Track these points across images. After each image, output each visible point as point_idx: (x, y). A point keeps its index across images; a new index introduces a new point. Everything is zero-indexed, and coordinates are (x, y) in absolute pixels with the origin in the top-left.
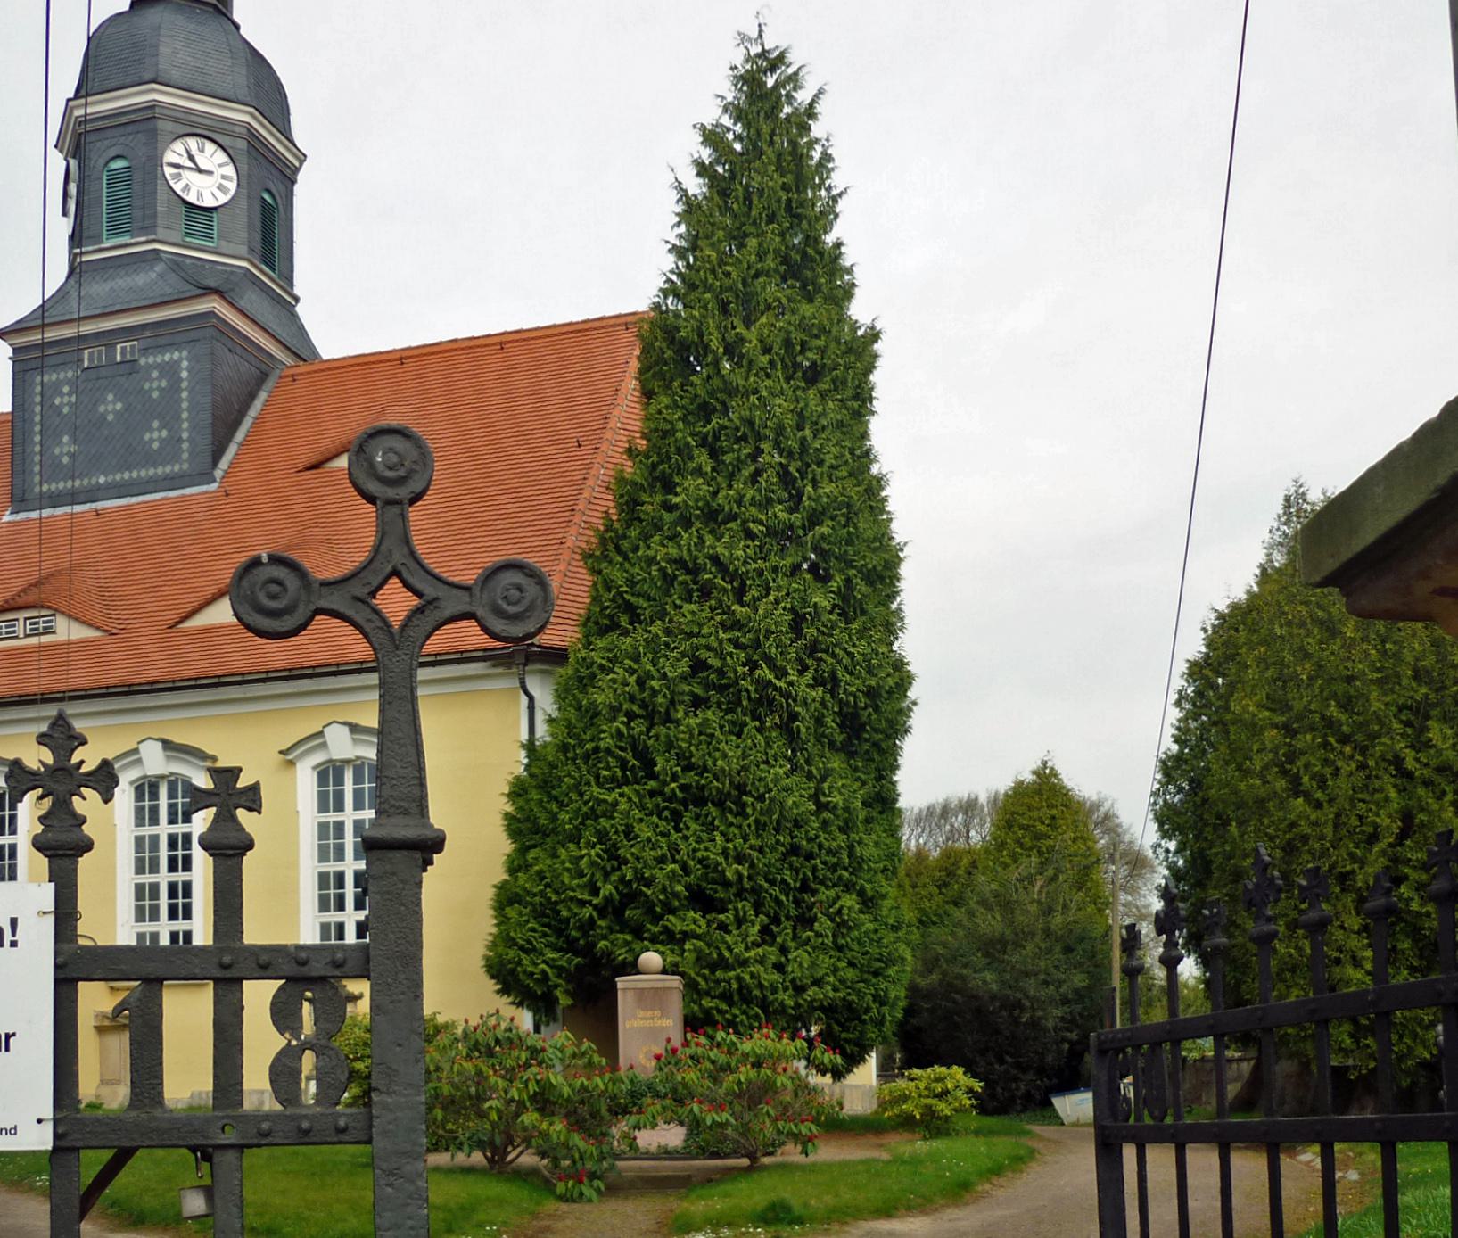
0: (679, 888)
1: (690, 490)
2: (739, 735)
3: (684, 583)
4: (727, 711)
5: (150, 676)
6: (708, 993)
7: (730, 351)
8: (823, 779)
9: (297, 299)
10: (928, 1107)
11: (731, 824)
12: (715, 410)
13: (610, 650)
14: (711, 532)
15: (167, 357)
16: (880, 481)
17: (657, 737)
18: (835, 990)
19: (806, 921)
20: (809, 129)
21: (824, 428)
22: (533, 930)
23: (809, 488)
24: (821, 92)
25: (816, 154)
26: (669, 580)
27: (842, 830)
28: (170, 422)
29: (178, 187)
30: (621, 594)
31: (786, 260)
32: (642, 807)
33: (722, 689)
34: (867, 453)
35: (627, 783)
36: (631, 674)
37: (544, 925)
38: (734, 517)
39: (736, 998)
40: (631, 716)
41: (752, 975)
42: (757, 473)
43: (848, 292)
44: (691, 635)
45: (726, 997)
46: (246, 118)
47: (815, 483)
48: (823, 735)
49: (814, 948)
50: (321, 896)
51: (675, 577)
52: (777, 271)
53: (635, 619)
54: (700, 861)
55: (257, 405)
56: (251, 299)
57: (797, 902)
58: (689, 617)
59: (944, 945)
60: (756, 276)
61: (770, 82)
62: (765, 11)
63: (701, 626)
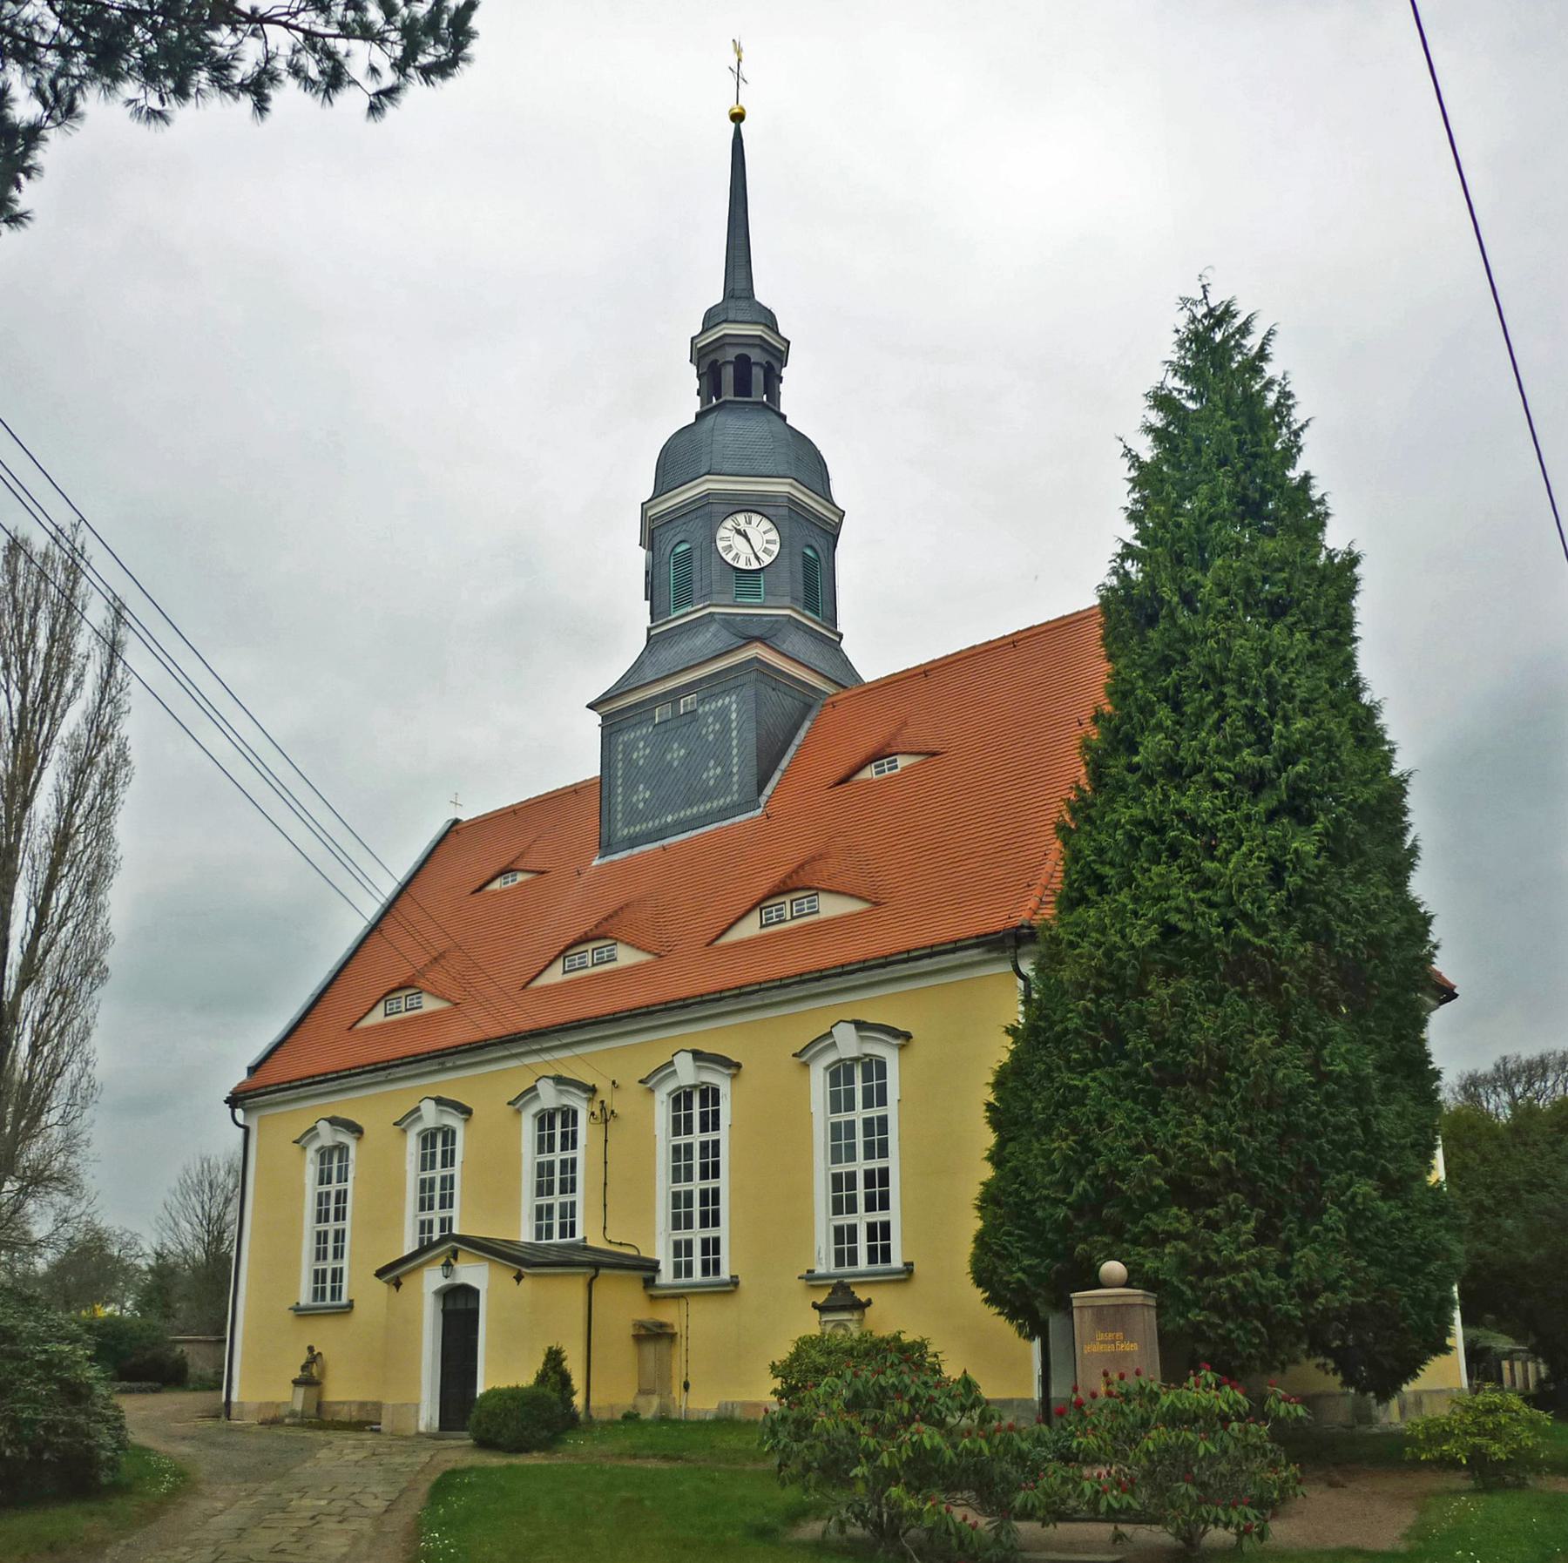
0: (1158, 1181)
1: (1152, 746)
2: (1218, 1004)
3: (1151, 845)
4: (1205, 978)
5: (683, 992)
6: (1196, 1303)
7: (1188, 600)
8: (1323, 1044)
10: (1476, 1449)
11: (1215, 1104)
12: (1174, 663)
13: (1078, 925)
14: (1176, 788)
15: (720, 703)
16: (1371, 712)
17: (1128, 1011)
18: (1355, 1294)
19: (1313, 1211)
20: (1262, 370)
21: (1292, 662)
22: (1009, 1234)
23: (1278, 727)
24: (1271, 333)
25: (1271, 398)
26: (1135, 842)
27: (1352, 1102)
28: (724, 762)
29: (729, 558)
30: (1088, 864)
31: (1243, 500)
32: (1115, 1091)
33: (1196, 955)
34: (1357, 680)
35: (1100, 1065)
36: (1099, 947)
37: (1021, 1228)
38: (1198, 769)
39: (1230, 1309)
40: (1099, 992)
41: (1246, 1282)
42: (1222, 719)
43: (1320, 523)
44: (1160, 899)
45: (1217, 1307)
46: (786, 489)
47: (1287, 721)
48: (1320, 995)
49: (1324, 1245)
50: (834, 1198)
51: (1142, 838)
52: (1234, 513)
53: (1103, 890)
54: (1181, 1148)
55: (802, 733)
56: (795, 643)
57: (1303, 1189)
58: (1157, 880)
59: (1550, 1213)
60: (1211, 520)
61: (1218, 337)
62: (1208, 273)
63: (1168, 887)
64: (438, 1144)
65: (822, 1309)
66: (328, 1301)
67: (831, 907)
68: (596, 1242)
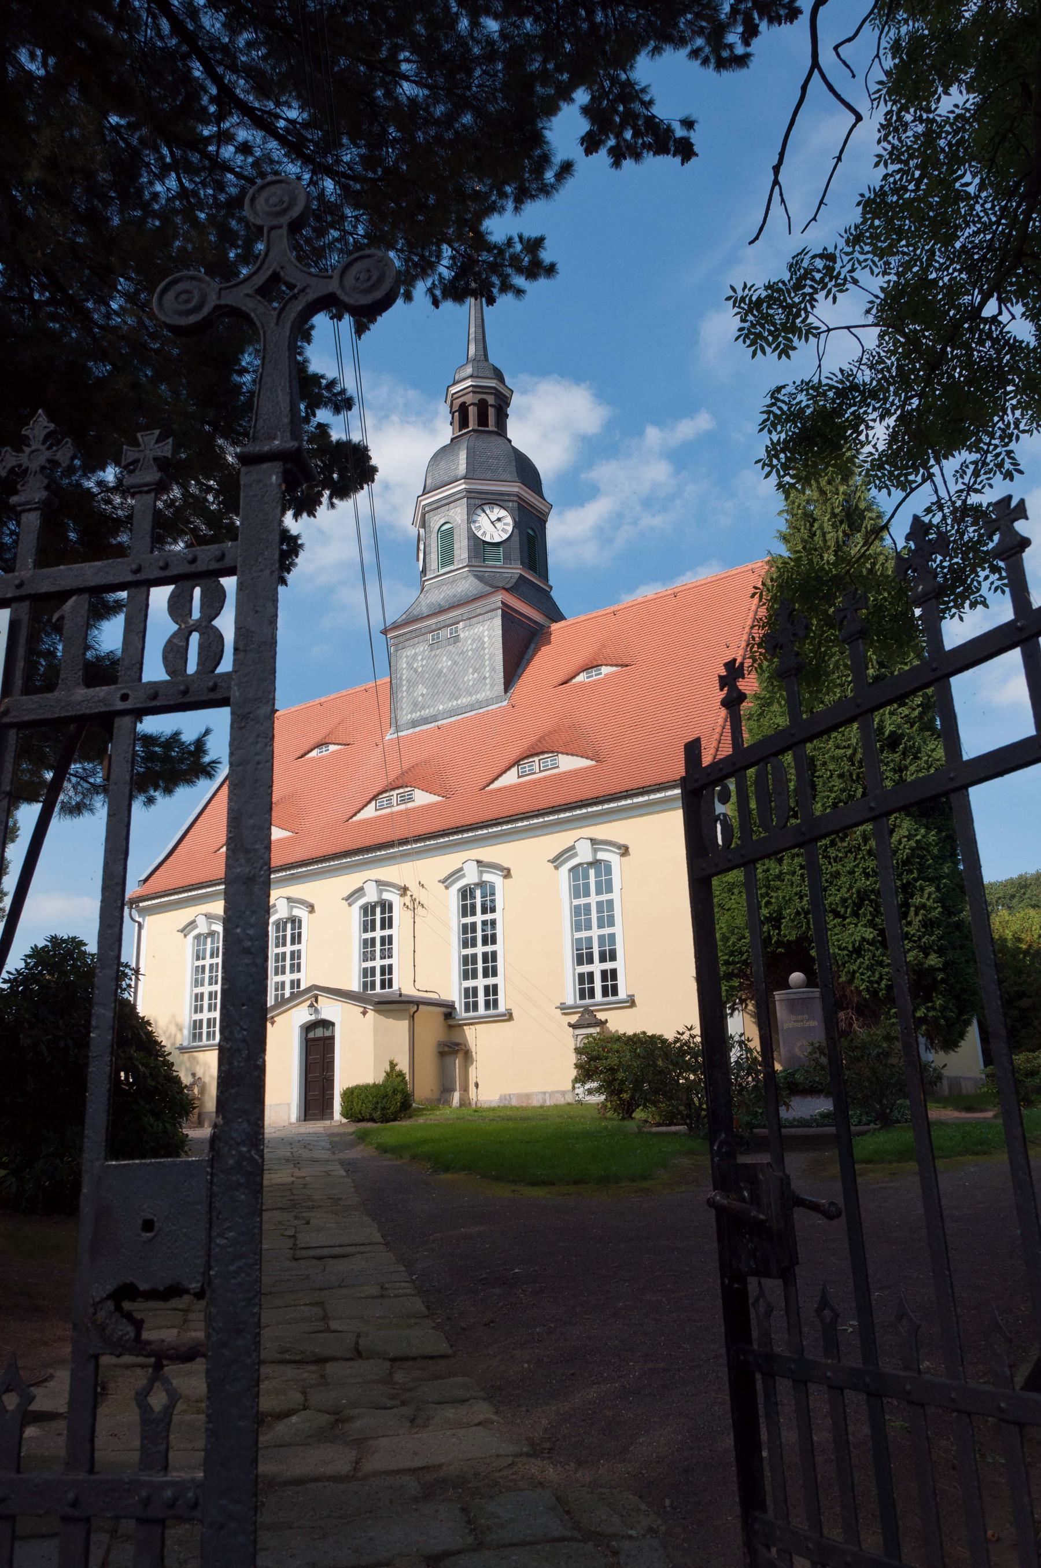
9: (551, 588)
46: (463, 486)
64: (377, 915)
65: (574, 1026)
66: (205, 1041)
67: (568, 763)
68: (409, 990)
